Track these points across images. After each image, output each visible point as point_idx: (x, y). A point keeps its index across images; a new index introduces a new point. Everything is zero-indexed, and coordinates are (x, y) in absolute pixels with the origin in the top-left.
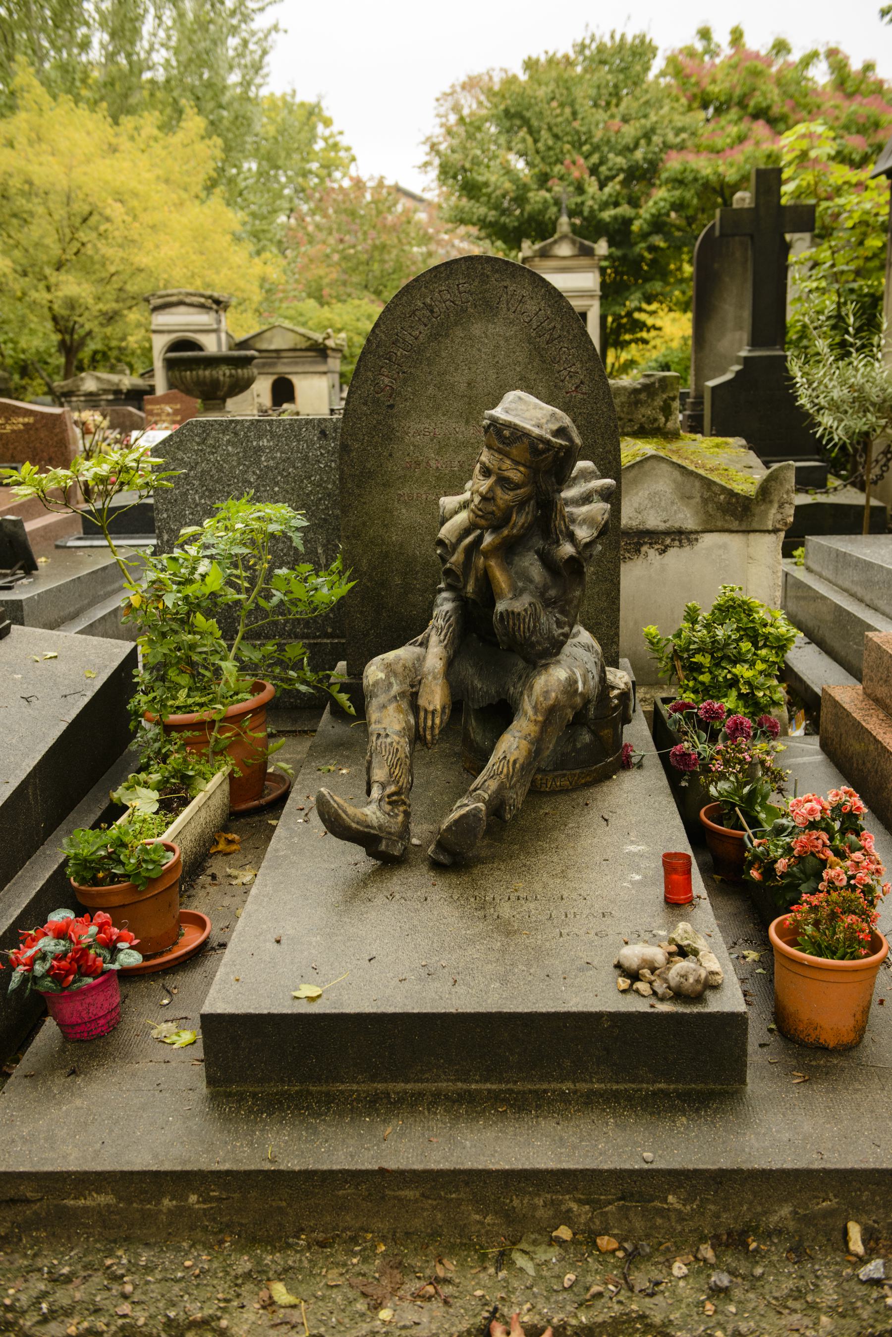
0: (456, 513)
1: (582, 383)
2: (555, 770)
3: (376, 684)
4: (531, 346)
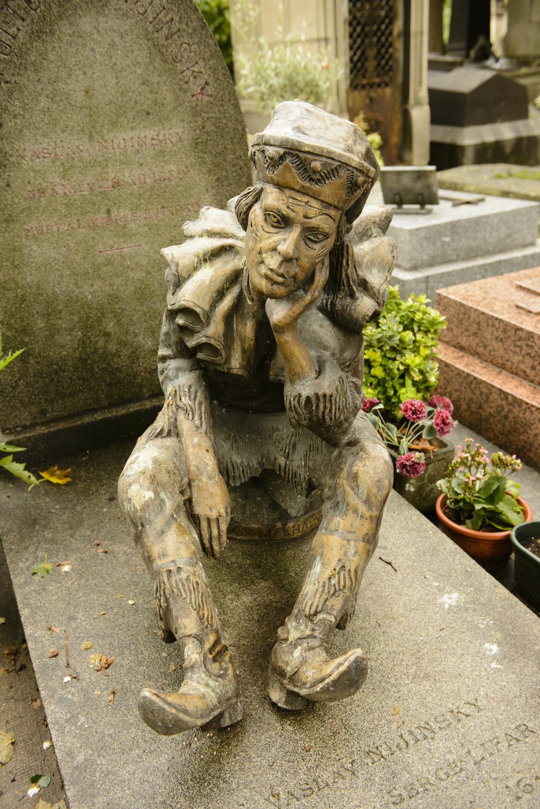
0: (196, 269)
1: (207, 84)
2: (306, 513)
3: (146, 506)
4: (150, 43)
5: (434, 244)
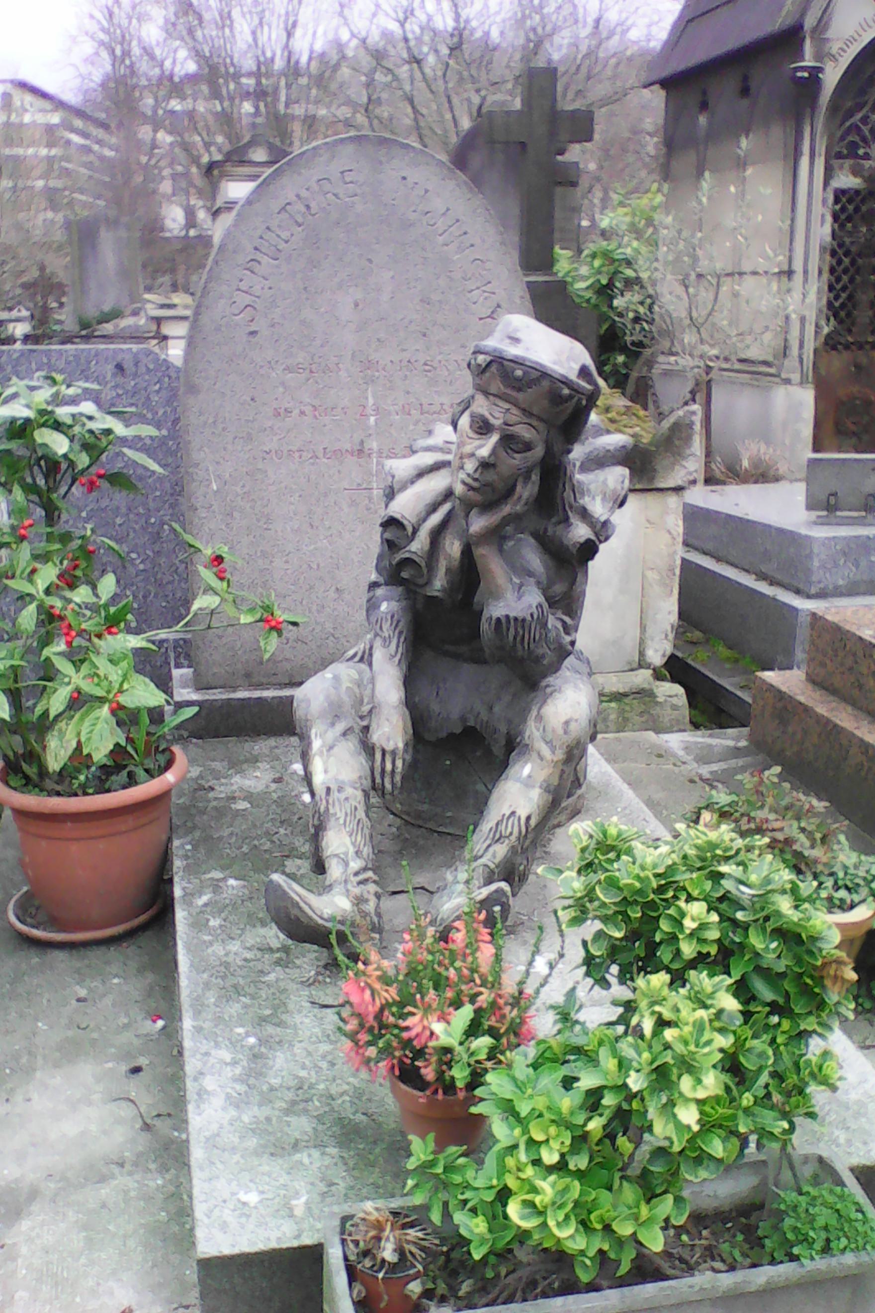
5: (857, 565)
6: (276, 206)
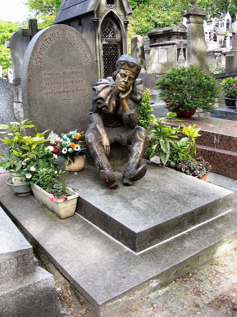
6: (44, 39)
